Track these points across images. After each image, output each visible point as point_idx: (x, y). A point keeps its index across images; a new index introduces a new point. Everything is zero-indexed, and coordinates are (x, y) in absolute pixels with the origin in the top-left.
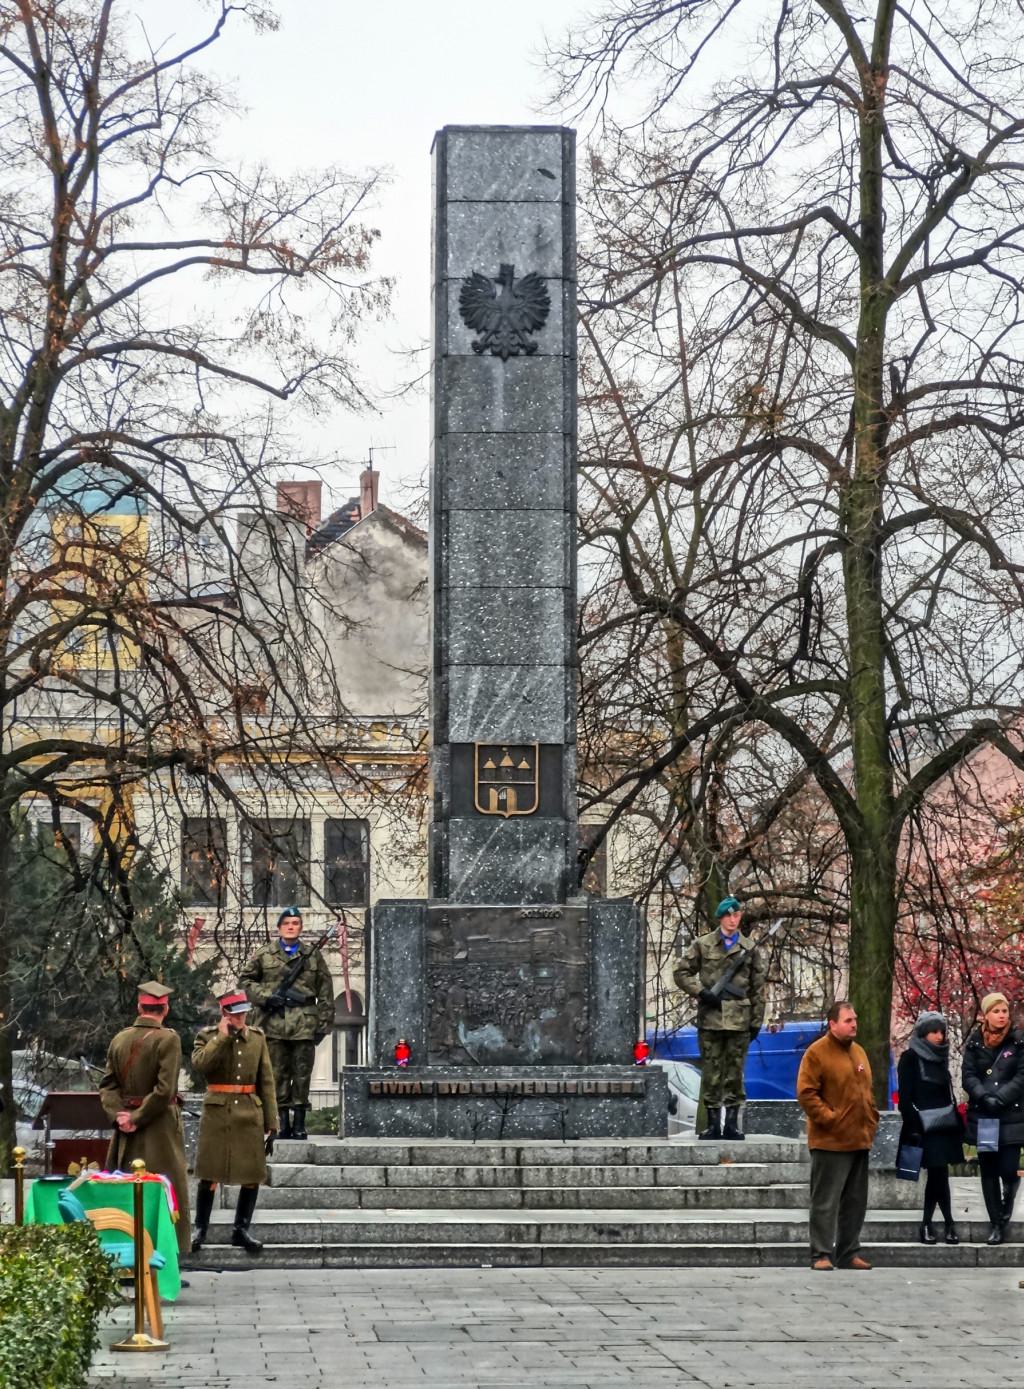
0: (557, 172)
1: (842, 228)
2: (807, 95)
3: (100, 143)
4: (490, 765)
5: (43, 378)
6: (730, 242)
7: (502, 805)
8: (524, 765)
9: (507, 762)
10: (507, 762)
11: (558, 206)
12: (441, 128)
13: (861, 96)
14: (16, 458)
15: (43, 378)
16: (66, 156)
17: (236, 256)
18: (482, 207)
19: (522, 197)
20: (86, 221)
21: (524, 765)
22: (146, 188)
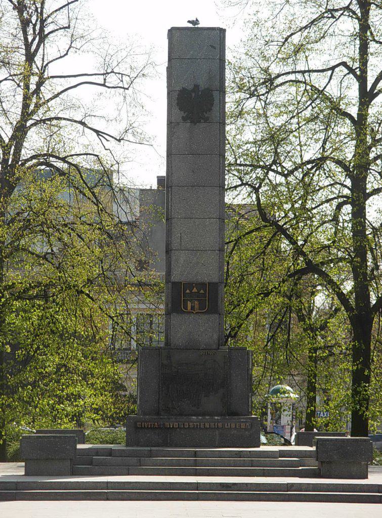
0: (218, 47)
1: (351, 71)
2: (337, 14)
3: (46, 33)
4: (188, 291)
5: (20, 131)
6: (102, 77)
7: (193, 308)
8: (202, 291)
9: (195, 290)
10: (195, 290)
11: (218, 61)
12: (221, 27)
13: (16, 3)
14: (10, 163)
15: (20, 131)
16: (30, 38)
17: (100, 79)
18: (186, 61)
19: (203, 57)
20: (40, 66)
21: (202, 291)
22: (65, 52)
